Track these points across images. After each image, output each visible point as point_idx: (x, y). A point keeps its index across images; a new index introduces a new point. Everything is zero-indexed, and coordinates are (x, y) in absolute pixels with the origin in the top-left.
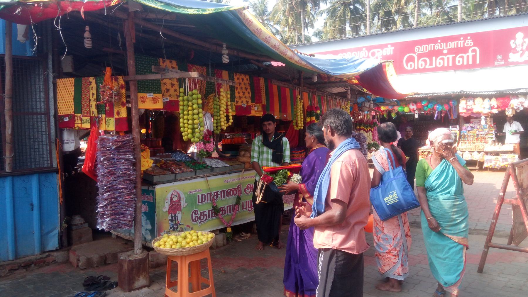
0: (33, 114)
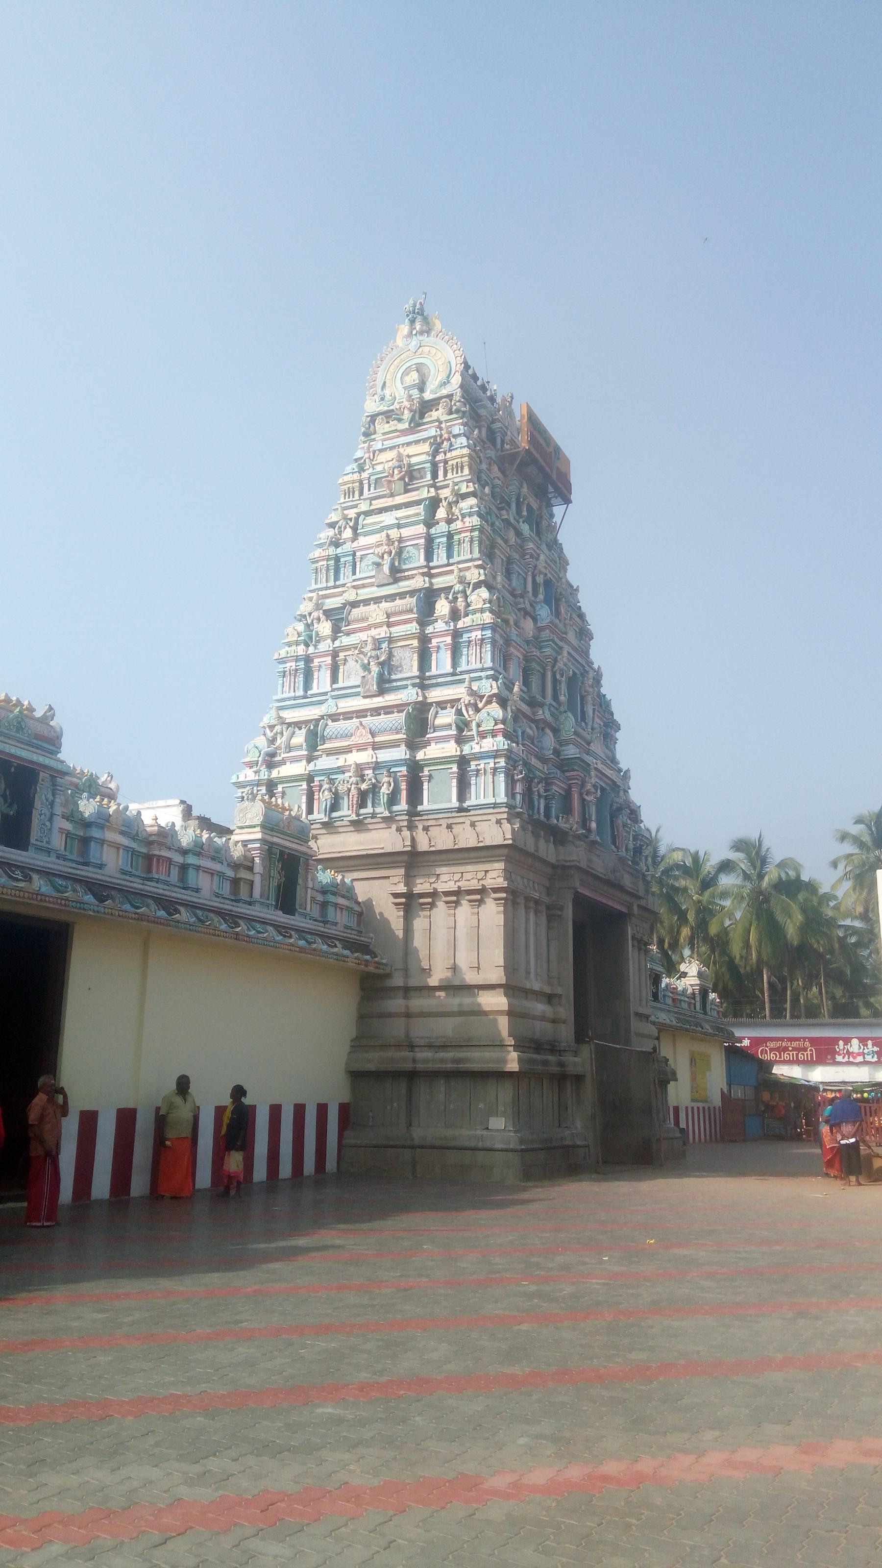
0: (674, 1044)
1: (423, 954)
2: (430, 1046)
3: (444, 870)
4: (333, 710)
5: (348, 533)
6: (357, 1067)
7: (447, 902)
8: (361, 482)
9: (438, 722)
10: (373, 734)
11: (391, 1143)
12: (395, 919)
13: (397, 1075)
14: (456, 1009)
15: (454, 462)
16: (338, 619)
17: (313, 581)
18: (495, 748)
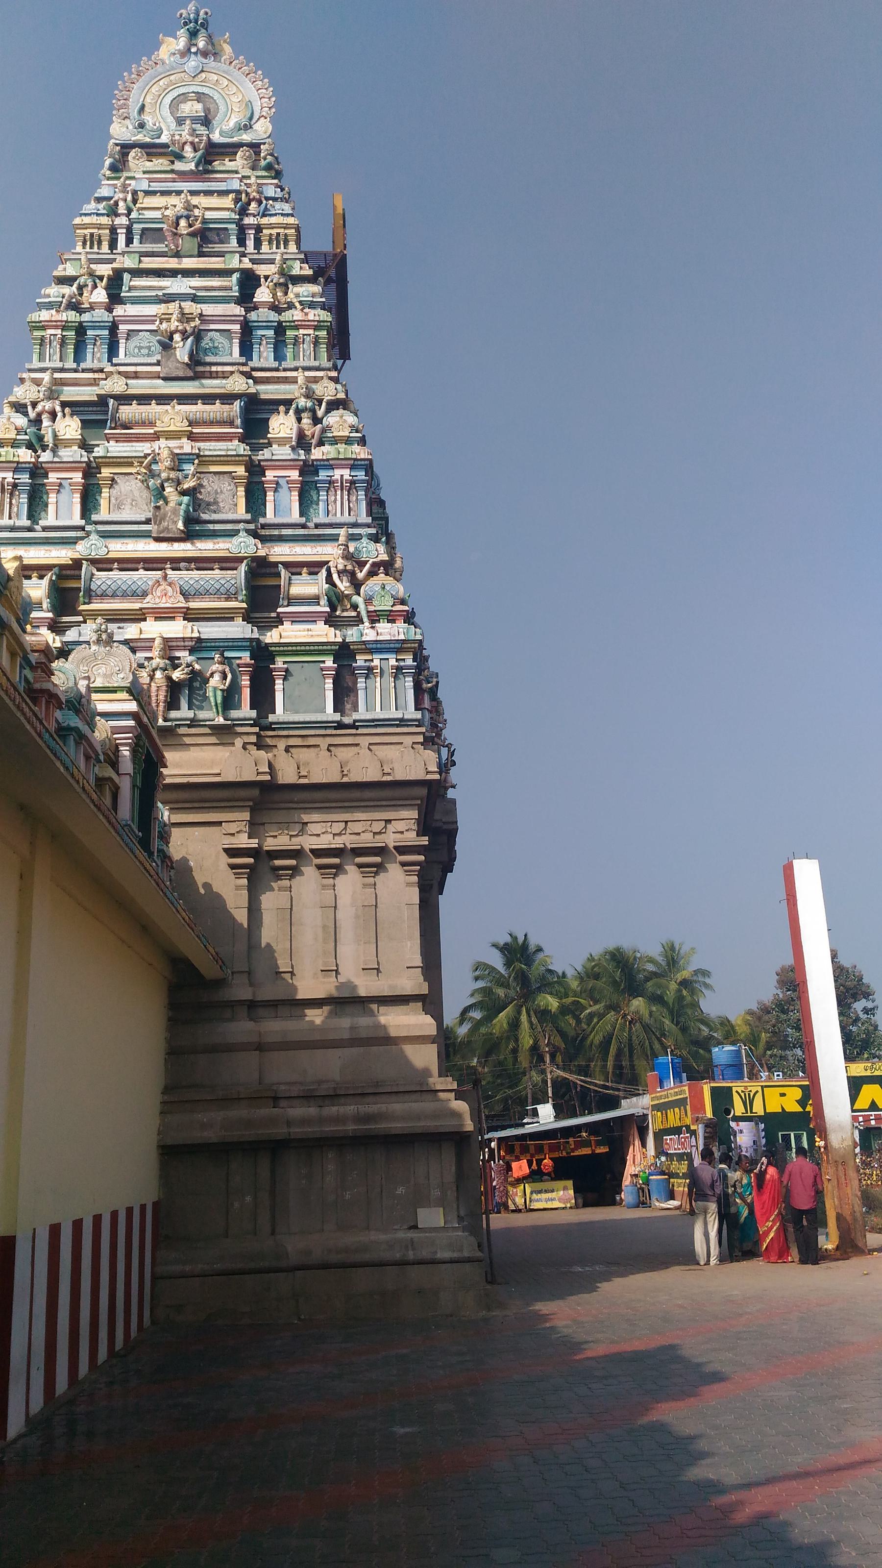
1: (280, 948)
2: (308, 1097)
3: (315, 817)
4: (101, 553)
5: (100, 295)
6: (169, 1142)
7: (319, 867)
8: (113, 230)
9: (295, 590)
10: (185, 595)
12: (232, 892)
13: (252, 1149)
14: (346, 1036)
15: (274, 232)
16: (96, 415)
17: (35, 357)
18: (402, 637)
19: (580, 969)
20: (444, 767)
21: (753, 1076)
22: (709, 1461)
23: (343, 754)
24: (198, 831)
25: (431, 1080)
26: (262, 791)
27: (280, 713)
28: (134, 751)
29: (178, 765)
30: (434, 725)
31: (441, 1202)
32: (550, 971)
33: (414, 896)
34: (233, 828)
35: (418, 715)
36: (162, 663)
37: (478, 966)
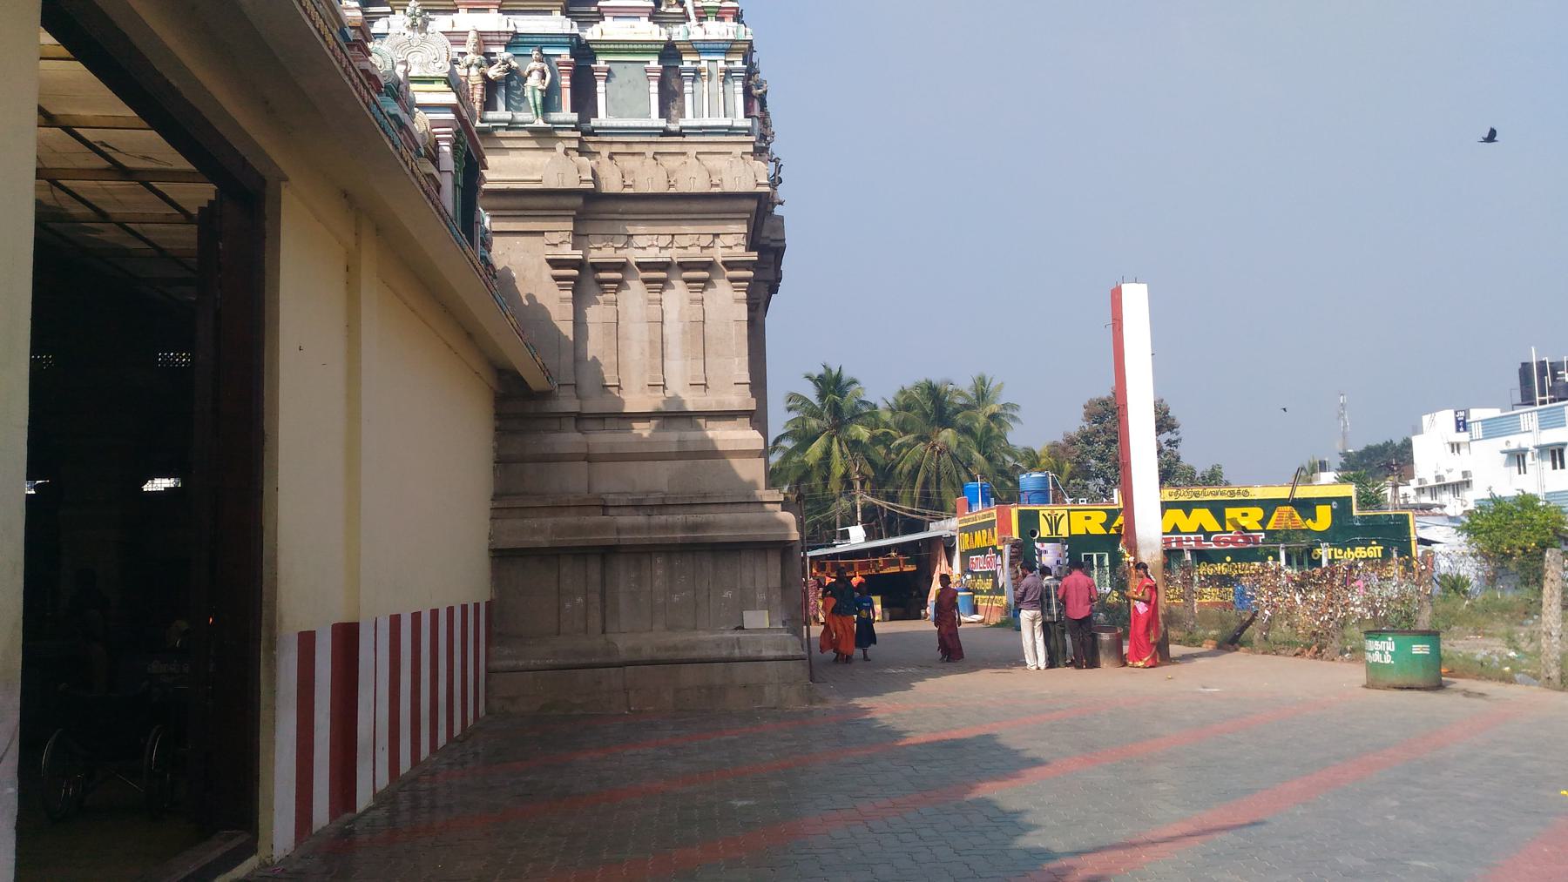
1: (607, 363)
2: (637, 506)
3: (641, 229)
7: (646, 281)
11: (584, 661)
12: (557, 303)
13: (582, 553)
14: (674, 449)
18: (731, 37)
19: (891, 401)
20: (775, 181)
21: (1058, 500)
22: (1037, 832)
23: (671, 163)
24: (519, 240)
25: (758, 492)
26: (585, 201)
27: (602, 119)
28: (454, 148)
29: (496, 170)
30: (763, 137)
31: (767, 605)
32: (864, 403)
33: (742, 312)
34: (556, 238)
35: (748, 123)
36: (477, 59)
37: (792, 397)
